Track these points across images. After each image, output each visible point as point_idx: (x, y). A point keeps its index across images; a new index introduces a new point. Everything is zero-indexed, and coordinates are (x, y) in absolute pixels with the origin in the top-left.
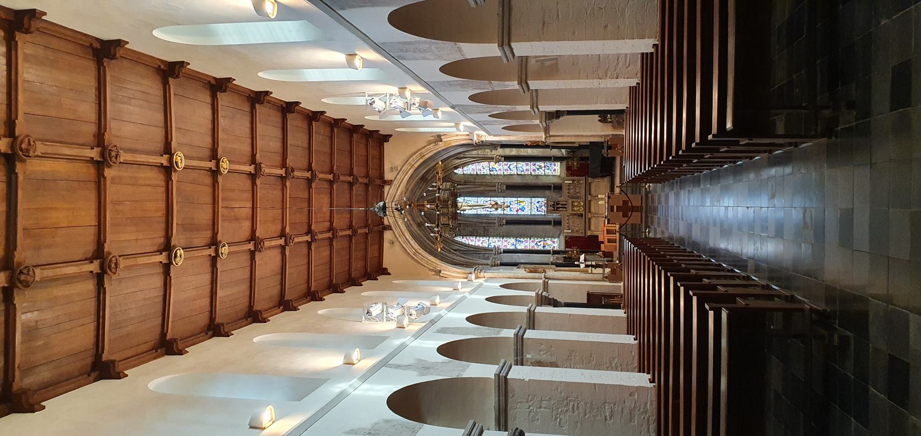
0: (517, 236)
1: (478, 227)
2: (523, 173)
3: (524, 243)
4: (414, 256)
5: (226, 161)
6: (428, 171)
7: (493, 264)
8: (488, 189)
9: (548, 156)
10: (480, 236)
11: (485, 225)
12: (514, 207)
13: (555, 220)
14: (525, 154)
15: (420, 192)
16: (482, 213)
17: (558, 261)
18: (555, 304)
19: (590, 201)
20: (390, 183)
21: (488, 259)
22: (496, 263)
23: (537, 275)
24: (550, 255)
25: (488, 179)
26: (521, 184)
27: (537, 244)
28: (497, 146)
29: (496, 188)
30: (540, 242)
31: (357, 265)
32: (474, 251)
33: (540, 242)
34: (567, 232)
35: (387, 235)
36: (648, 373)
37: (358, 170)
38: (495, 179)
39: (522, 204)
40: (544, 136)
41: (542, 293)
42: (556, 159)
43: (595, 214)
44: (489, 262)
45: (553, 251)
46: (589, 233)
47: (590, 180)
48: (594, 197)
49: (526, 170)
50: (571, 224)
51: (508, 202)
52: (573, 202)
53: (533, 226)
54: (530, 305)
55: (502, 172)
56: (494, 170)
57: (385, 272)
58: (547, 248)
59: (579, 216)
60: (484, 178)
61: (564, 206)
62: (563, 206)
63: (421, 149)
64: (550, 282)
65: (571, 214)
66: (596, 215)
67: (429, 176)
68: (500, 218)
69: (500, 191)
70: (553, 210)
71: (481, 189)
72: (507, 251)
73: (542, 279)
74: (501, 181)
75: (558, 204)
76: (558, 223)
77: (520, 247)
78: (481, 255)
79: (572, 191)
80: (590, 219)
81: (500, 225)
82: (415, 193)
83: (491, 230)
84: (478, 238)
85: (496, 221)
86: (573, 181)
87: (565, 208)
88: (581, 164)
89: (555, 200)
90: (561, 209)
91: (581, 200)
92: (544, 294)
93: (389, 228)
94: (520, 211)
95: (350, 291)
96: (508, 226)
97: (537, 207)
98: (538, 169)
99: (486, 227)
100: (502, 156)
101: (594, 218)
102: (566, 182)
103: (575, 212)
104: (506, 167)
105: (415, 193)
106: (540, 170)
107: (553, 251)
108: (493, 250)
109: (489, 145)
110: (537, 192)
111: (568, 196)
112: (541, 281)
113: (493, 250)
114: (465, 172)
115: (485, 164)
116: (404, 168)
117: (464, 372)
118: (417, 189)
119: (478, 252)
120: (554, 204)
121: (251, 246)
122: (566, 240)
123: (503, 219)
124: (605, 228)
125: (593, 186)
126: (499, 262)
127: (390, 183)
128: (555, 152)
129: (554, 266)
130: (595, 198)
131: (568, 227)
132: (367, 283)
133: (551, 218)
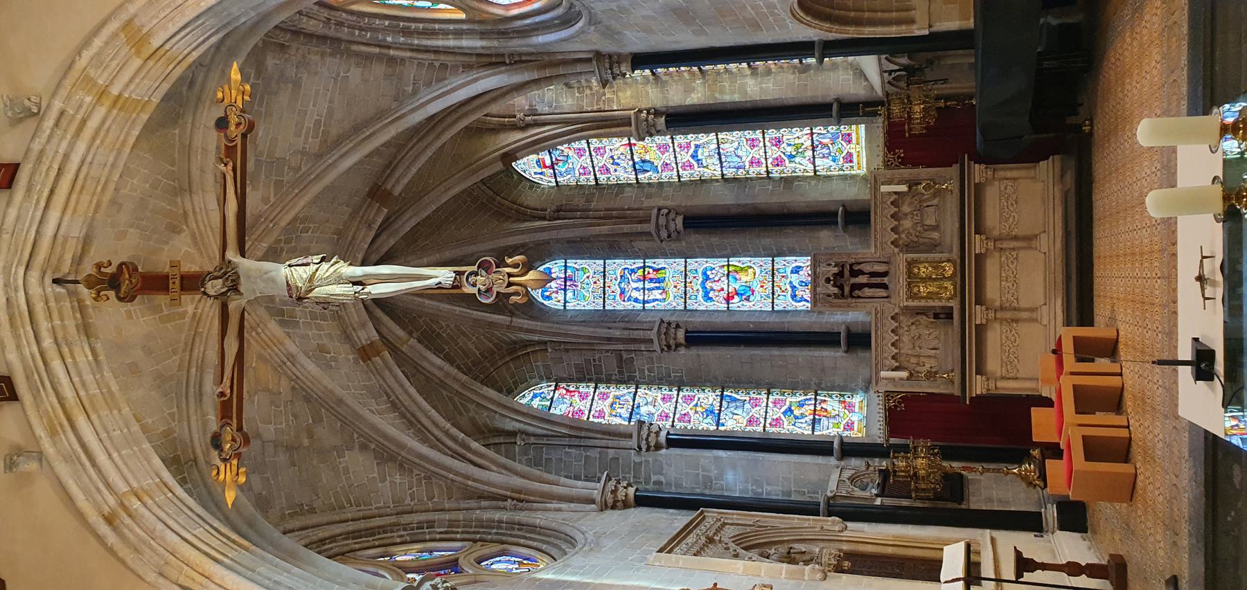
0: (724, 383)
1: (600, 351)
2: (741, 173)
3: (747, 406)
4: (104, 529)
8: (627, 228)
9: (820, 100)
10: (608, 381)
11: (621, 347)
12: (716, 286)
13: (853, 330)
14: (737, 98)
16: (619, 308)
17: (858, 493)
19: (980, 259)
22: (621, 495)
24: (832, 461)
25: (629, 197)
26: (734, 211)
27: (790, 410)
28: (619, 63)
29: (651, 227)
30: (801, 405)
32: (570, 436)
33: (801, 405)
34: (892, 380)
38: (649, 196)
39: (744, 278)
42: (848, 110)
43: (1002, 308)
45: (842, 443)
46: (979, 387)
47: (979, 172)
49: (752, 163)
50: (906, 348)
51: (700, 271)
52: (911, 264)
53: (776, 352)
55: (675, 173)
59: (936, 316)
60: (617, 195)
61: (879, 281)
65: (906, 308)
66: (1008, 315)
67: (398, 181)
68: (667, 325)
69: (664, 234)
70: (836, 296)
71: (605, 229)
74: (669, 203)
76: (858, 340)
77: (735, 422)
79: (907, 224)
80: (981, 330)
81: (669, 347)
83: (640, 363)
84: (602, 388)
85: (653, 335)
86: (912, 184)
87: (885, 286)
88: (939, 109)
90: (867, 291)
91: (945, 255)
94: (736, 299)
96: (694, 351)
97: (793, 287)
99: (625, 356)
100: (657, 113)
101: (997, 326)
102: (884, 189)
103: (923, 303)
104: (685, 157)
106: (797, 160)
107: (842, 443)
108: (630, 436)
109: (588, 60)
110: (791, 237)
113: (630, 436)
115: (617, 145)
120: (840, 274)
123: (678, 326)
124: (1067, 383)
125: (992, 196)
126: (631, 491)
130: (999, 245)
131: (893, 358)
133: (838, 324)
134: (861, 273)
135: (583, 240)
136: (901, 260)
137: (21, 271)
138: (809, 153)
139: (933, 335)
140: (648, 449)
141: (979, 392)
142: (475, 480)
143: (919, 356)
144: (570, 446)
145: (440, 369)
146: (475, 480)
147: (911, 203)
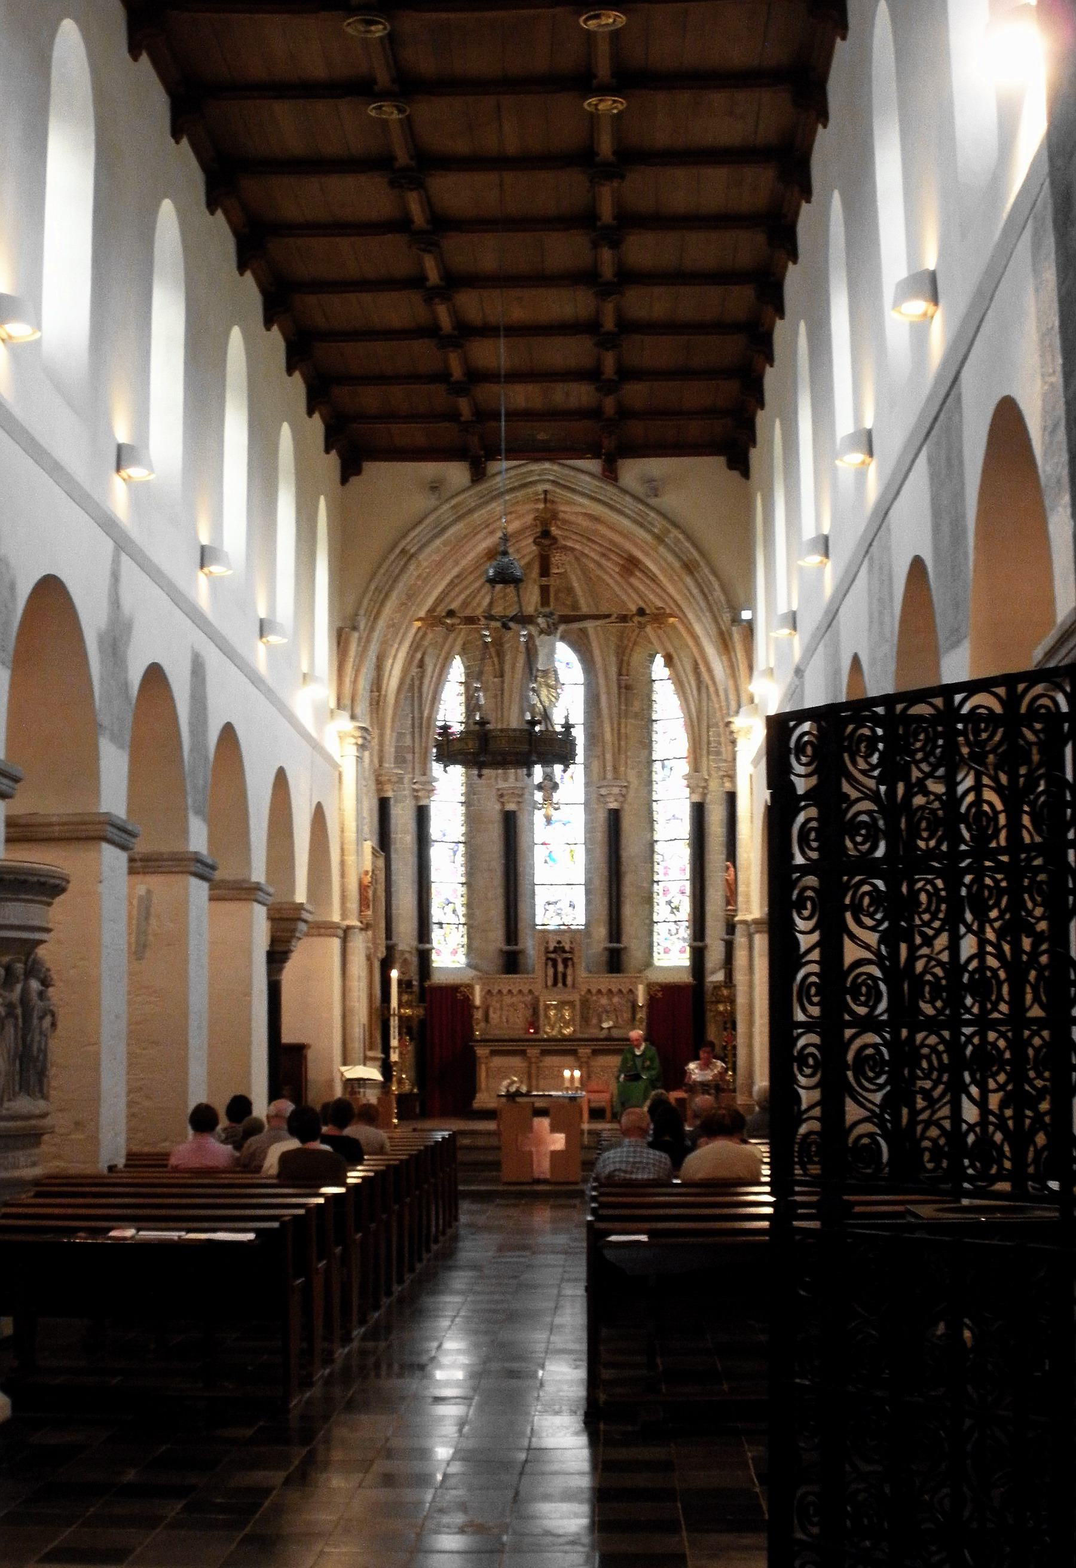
4: (397, 551)
5: (616, 108)
6: (653, 578)
7: (384, 779)
13: (520, 956)
15: (592, 554)
18: (277, 957)
20: (610, 474)
21: (400, 760)
23: (353, 905)
24: (415, 943)
30: (454, 911)
31: (370, 398)
32: (421, 718)
35: (456, 473)
36: (126, 1166)
37: (636, 393)
40: (749, 917)
41: (305, 921)
42: (698, 955)
44: (389, 764)
46: (481, 1051)
48: (587, 1063)
52: (571, 1004)
54: (271, 890)
56: (667, 770)
57: (349, 469)
58: (436, 934)
60: (641, 742)
62: (560, 976)
63: (709, 563)
64: (336, 943)
69: (603, 791)
71: (608, 736)
72: (422, 815)
73: (343, 919)
75: (565, 961)
76: (512, 962)
78: (408, 741)
79: (604, 1001)
81: (502, 796)
82: (589, 539)
87: (555, 984)
89: (577, 954)
90: (551, 972)
91: (578, 1028)
92: (302, 926)
93: (478, 475)
95: (296, 386)
97: (556, 903)
98: (669, 903)
105: (589, 539)
111: (589, 991)
112: (336, 918)
114: (656, 686)
116: (652, 514)
117: (111, 740)
118: (601, 545)
119: (416, 730)
120: (564, 951)
121: (402, 157)
122: (461, 985)
126: (390, 794)
127: (610, 474)
128: (715, 954)
129: (382, 953)
131: (510, 991)
132: (316, 426)
134: (566, 966)
135: (599, 715)
136: (576, 997)
137: (551, 478)
138: (673, 918)
139: (517, 1020)
140: (415, 790)
141: (478, 1051)
142: (392, 665)
143: (501, 1009)
144: (413, 718)
145: (479, 605)
146: (392, 665)
147: (620, 1003)
